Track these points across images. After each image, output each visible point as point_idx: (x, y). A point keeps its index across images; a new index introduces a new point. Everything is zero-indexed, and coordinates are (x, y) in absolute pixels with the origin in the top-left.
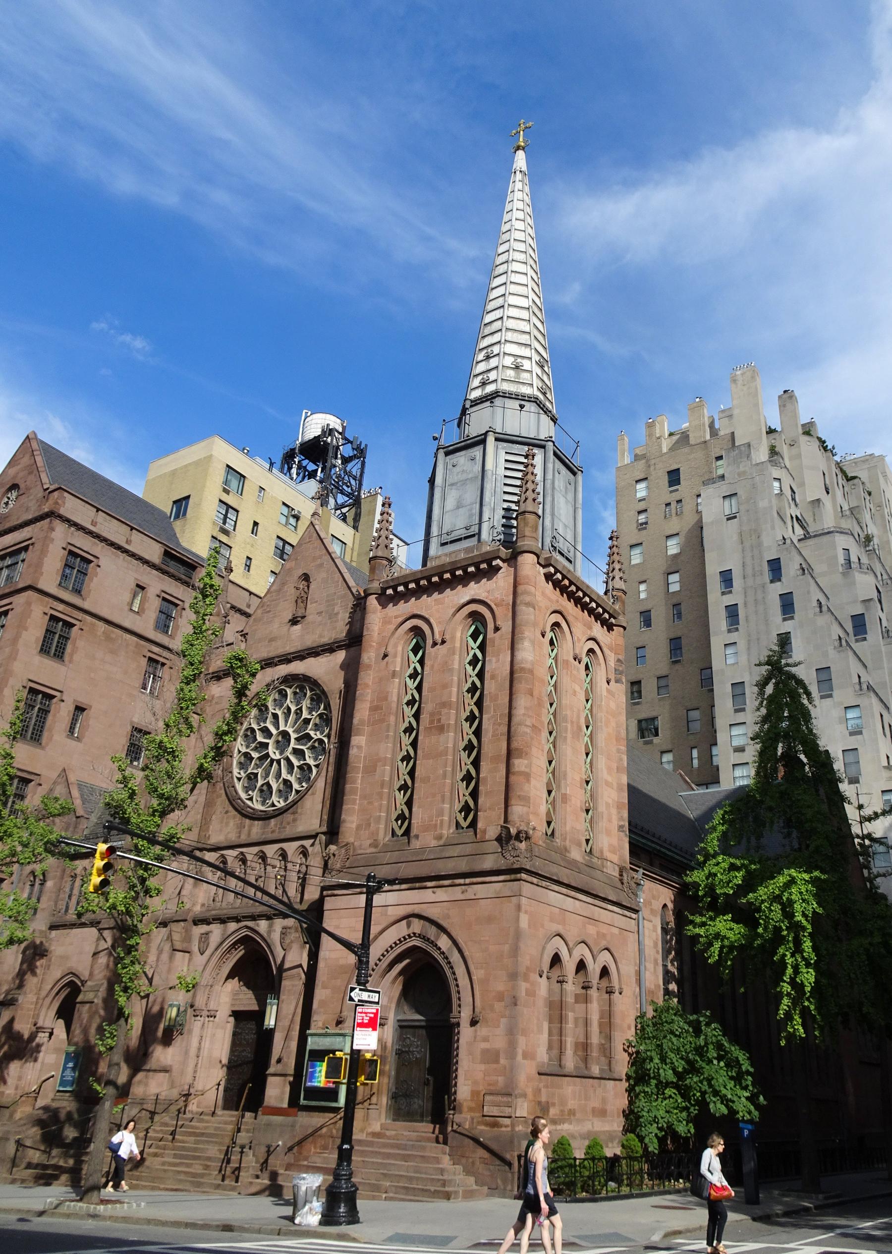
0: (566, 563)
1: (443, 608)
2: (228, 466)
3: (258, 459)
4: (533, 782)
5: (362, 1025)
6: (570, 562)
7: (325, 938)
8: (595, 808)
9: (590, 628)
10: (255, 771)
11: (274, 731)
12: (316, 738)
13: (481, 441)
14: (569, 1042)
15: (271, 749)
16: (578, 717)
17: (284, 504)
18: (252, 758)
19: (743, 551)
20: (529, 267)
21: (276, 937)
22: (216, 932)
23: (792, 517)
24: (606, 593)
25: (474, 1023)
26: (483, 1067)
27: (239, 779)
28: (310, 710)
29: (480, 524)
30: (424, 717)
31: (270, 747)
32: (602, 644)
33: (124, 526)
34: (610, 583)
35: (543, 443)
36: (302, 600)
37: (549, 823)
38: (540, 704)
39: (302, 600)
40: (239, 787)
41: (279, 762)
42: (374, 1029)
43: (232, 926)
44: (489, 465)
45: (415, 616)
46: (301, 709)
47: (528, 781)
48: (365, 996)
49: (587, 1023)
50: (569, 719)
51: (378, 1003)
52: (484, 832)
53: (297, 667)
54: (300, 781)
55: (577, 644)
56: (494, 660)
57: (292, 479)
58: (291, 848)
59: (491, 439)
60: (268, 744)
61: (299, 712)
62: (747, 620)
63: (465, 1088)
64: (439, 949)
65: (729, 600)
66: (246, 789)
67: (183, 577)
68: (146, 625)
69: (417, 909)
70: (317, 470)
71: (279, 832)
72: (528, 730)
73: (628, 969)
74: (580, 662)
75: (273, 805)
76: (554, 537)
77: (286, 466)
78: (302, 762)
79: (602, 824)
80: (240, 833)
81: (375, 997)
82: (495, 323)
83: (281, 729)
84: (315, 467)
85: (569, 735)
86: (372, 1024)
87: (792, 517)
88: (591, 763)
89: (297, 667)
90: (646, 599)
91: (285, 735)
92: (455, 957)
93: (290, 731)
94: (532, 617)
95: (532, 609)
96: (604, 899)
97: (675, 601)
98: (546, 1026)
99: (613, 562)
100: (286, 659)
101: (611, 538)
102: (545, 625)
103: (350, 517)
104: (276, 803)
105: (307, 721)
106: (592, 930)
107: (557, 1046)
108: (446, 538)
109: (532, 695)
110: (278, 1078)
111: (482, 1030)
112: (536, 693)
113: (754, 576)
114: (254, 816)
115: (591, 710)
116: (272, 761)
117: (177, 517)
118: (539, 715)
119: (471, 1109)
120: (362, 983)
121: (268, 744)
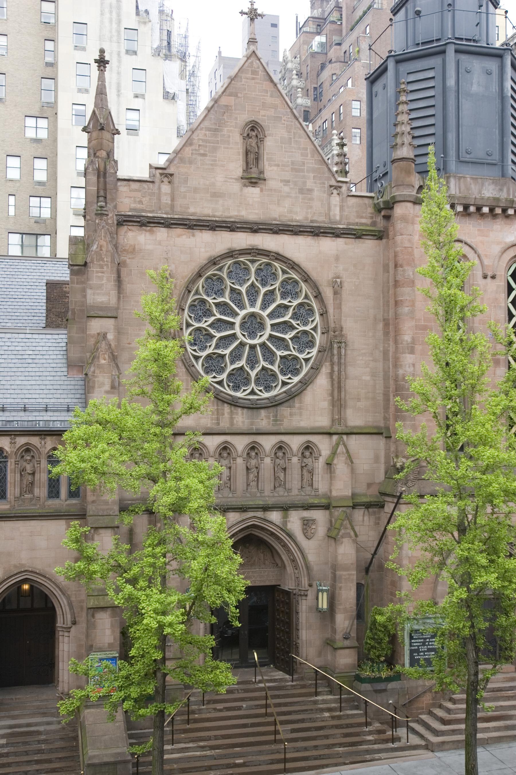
59: (451, 50)
80: (218, 419)
100: (254, 228)
110: (347, 651)
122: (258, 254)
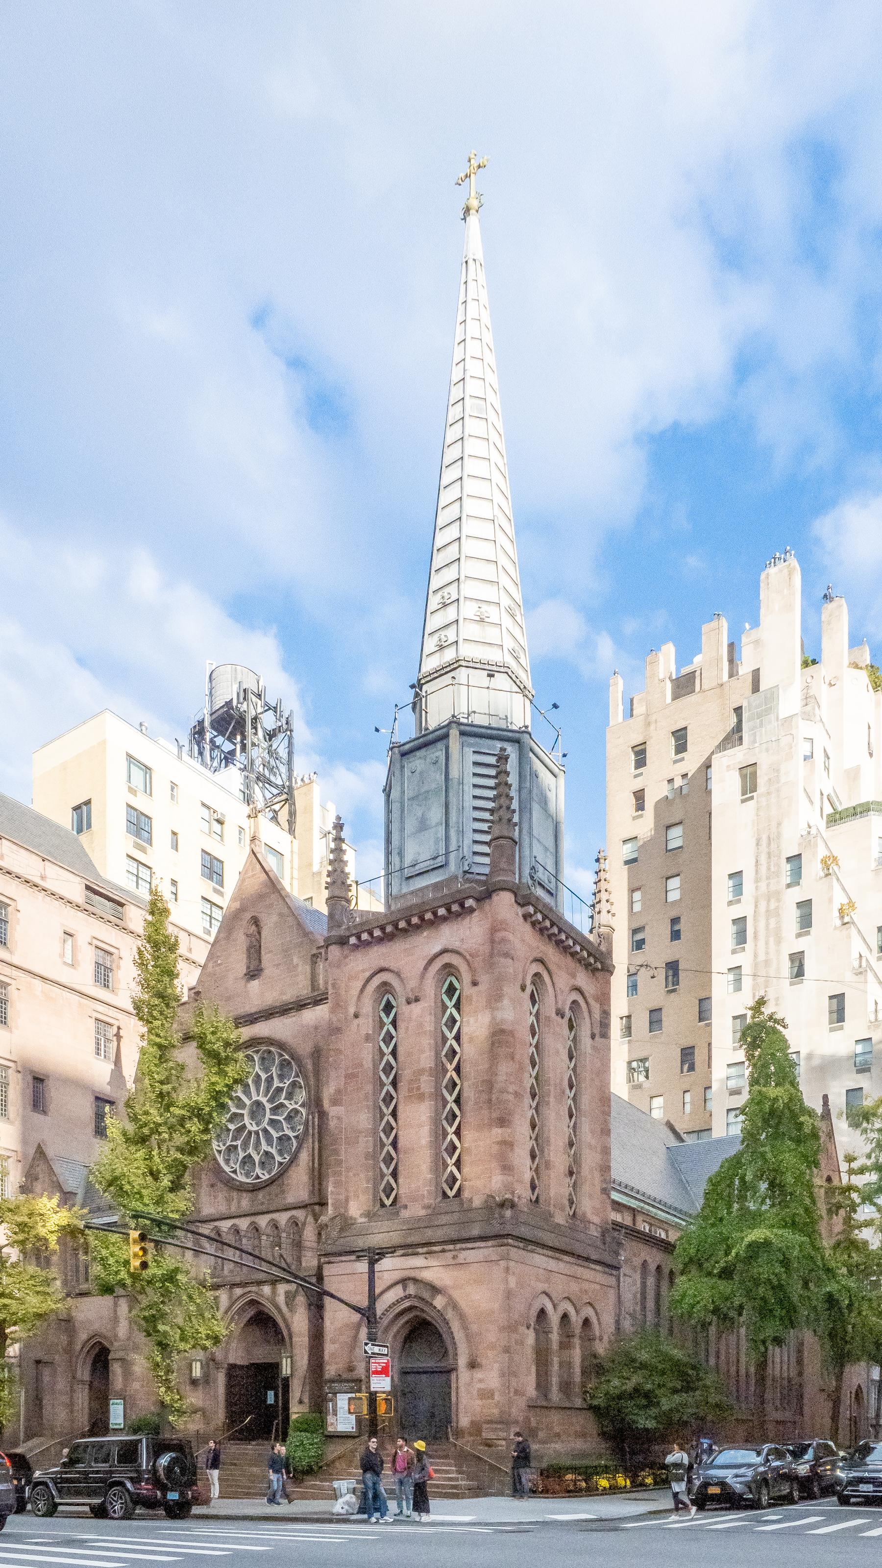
0: (547, 898)
1: (412, 956)
2: (129, 756)
3: (162, 741)
4: (517, 1150)
5: (376, 1372)
6: (551, 894)
7: (327, 1300)
8: (579, 1173)
9: (573, 976)
10: (234, 1143)
11: (248, 1102)
12: (291, 1107)
13: (440, 737)
14: (555, 1380)
15: (247, 1120)
16: (562, 1080)
17: (204, 805)
18: (229, 1130)
19: (757, 844)
20: (495, 487)
21: (281, 1299)
22: (224, 1297)
23: (822, 794)
24: (591, 932)
25: (473, 1365)
26: (479, 1402)
27: (220, 1152)
28: (281, 1077)
29: (447, 853)
30: (402, 1085)
31: (246, 1118)
32: (587, 995)
33: (34, 856)
34: (596, 917)
35: (517, 735)
36: (255, 950)
37: (533, 1187)
38: (521, 1068)
39: (255, 950)
40: (221, 1160)
41: (257, 1133)
42: (387, 1376)
43: (238, 1291)
44: (454, 773)
45: (382, 970)
46: (271, 1077)
47: (512, 1149)
48: (376, 1350)
49: (570, 1365)
50: (552, 1082)
51: (387, 1355)
52: (471, 1200)
53: (262, 1029)
54: (280, 1152)
55: (560, 997)
56: (472, 1020)
57: (203, 763)
58: (283, 1218)
59: (454, 733)
60: (243, 1115)
61: (270, 1080)
62: (756, 937)
63: (466, 1419)
64: (435, 1308)
65: (737, 912)
66: (227, 1161)
67: (112, 919)
68: (84, 977)
69: (412, 1274)
70: (234, 750)
71: (268, 1204)
72: (511, 1097)
73: (608, 1320)
74: (562, 1018)
75: (258, 1177)
76: (533, 868)
77: (196, 747)
78: (281, 1134)
79: (586, 1188)
81: (385, 1351)
82: (450, 548)
83: (254, 1099)
84: (232, 747)
85: (552, 1099)
86: (384, 1371)
87: (822, 794)
88: (575, 1127)
89: (262, 1029)
90: (640, 912)
91: (258, 1104)
92: (450, 1315)
93: (264, 1100)
94: (511, 971)
95: (511, 961)
96: (587, 1259)
97: (673, 914)
98: (533, 1369)
99: (600, 891)
101: (598, 860)
102: (524, 979)
103: (283, 816)
104: (261, 1176)
105: (279, 1090)
106: (574, 1287)
107: (542, 1385)
108: (407, 873)
109: (513, 1058)
111: (478, 1374)
112: (517, 1057)
113: (768, 878)
114: (241, 1188)
115: (574, 1070)
116: (250, 1133)
117: (80, 830)
118: (521, 1081)
119: (471, 1434)
120: (372, 1338)
121: (243, 1115)
122: (259, 1043)
